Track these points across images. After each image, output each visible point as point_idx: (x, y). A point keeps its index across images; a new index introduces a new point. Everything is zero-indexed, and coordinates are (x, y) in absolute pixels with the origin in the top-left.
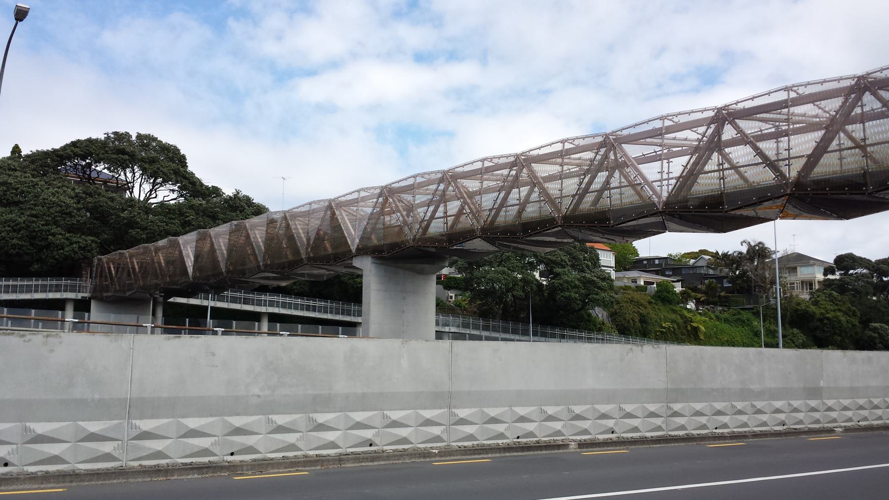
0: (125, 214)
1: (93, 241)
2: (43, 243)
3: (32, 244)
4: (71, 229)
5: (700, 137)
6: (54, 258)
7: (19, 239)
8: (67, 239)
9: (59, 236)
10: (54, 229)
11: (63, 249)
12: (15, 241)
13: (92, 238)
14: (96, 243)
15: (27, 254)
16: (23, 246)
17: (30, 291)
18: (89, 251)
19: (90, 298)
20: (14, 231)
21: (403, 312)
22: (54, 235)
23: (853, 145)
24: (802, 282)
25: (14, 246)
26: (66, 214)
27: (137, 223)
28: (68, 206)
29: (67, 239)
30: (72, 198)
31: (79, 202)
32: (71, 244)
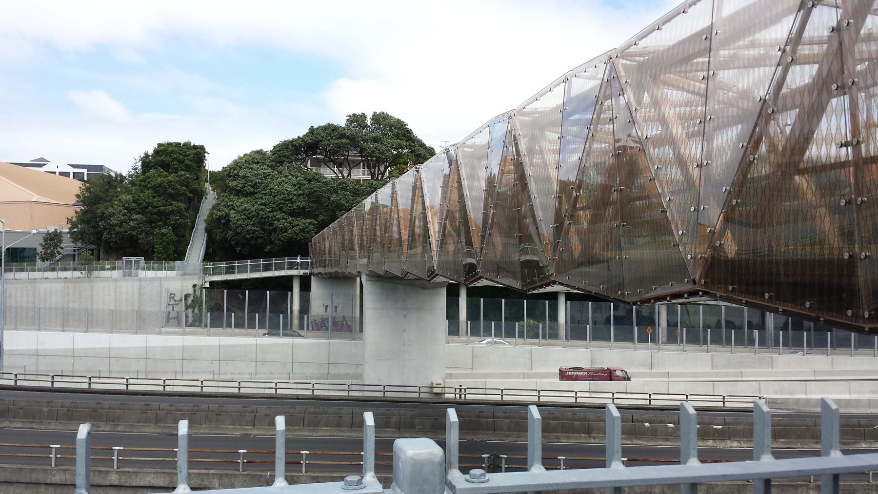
0: (334, 198)
1: (310, 223)
2: (271, 228)
3: (262, 229)
4: (291, 214)
5: (705, 73)
6: (279, 240)
7: (253, 225)
8: (290, 223)
9: (282, 221)
10: (279, 215)
11: (286, 231)
12: (249, 228)
13: (309, 221)
14: (314, 224)
15: (261, 238)
16: (255, 231)
17: (271, 270)
18: (308, 233)
19: (311, 274)
20: (249, 218)
21: (404, 330)
22: (278, 220)
23: (806, 34)
24: (752, 424)
25: (249, 232)
26: (288, 200)
27: (343, 205)
28: (289, 194)
29: (290, 223)
30: (295, 186)
31: (300, 188)
32: (293, 227)
